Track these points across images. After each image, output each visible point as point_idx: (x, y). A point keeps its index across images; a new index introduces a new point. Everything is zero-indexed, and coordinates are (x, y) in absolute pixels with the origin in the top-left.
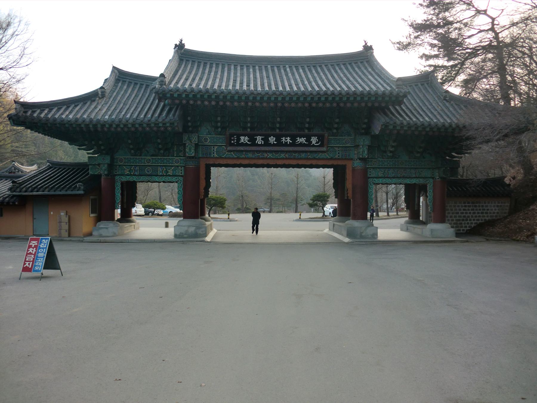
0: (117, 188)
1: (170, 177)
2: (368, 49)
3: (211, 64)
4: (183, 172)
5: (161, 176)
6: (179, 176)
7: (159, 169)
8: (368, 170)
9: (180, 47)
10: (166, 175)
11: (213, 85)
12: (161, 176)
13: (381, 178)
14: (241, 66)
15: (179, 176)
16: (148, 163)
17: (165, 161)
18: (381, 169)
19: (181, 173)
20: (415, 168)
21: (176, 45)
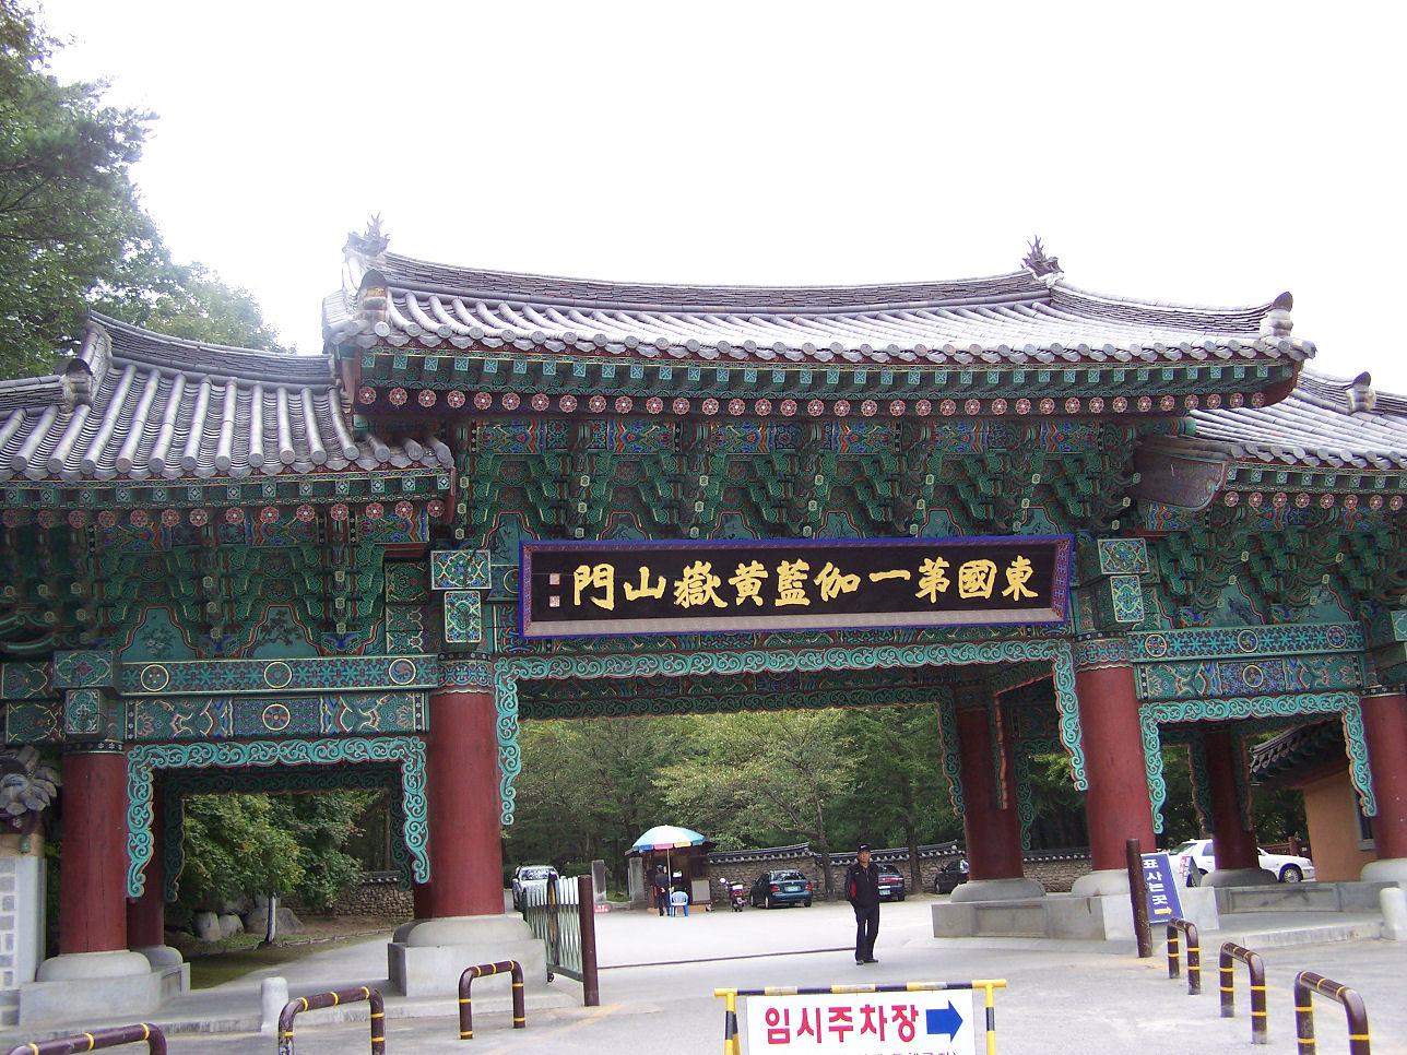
0: (135, 802)
1: (369, 744)
2: (1040, 263)
3: (164, 375)
4: (424, 715)
5: (334, 736)
6: (408, 734)
7: (325, 708)
8: (1137, 673)
9: (370, 244)
10: (353, 735)
11: (179, 445)
12: (334, 736)
13: (1181, 700)
14: (266, 390)
15: (408, 734)
16: (401, 677)
17: (351, 672)
18: (185, 705)
19: (419, 721)
20: (1296, 656)
21: (355, 241)
